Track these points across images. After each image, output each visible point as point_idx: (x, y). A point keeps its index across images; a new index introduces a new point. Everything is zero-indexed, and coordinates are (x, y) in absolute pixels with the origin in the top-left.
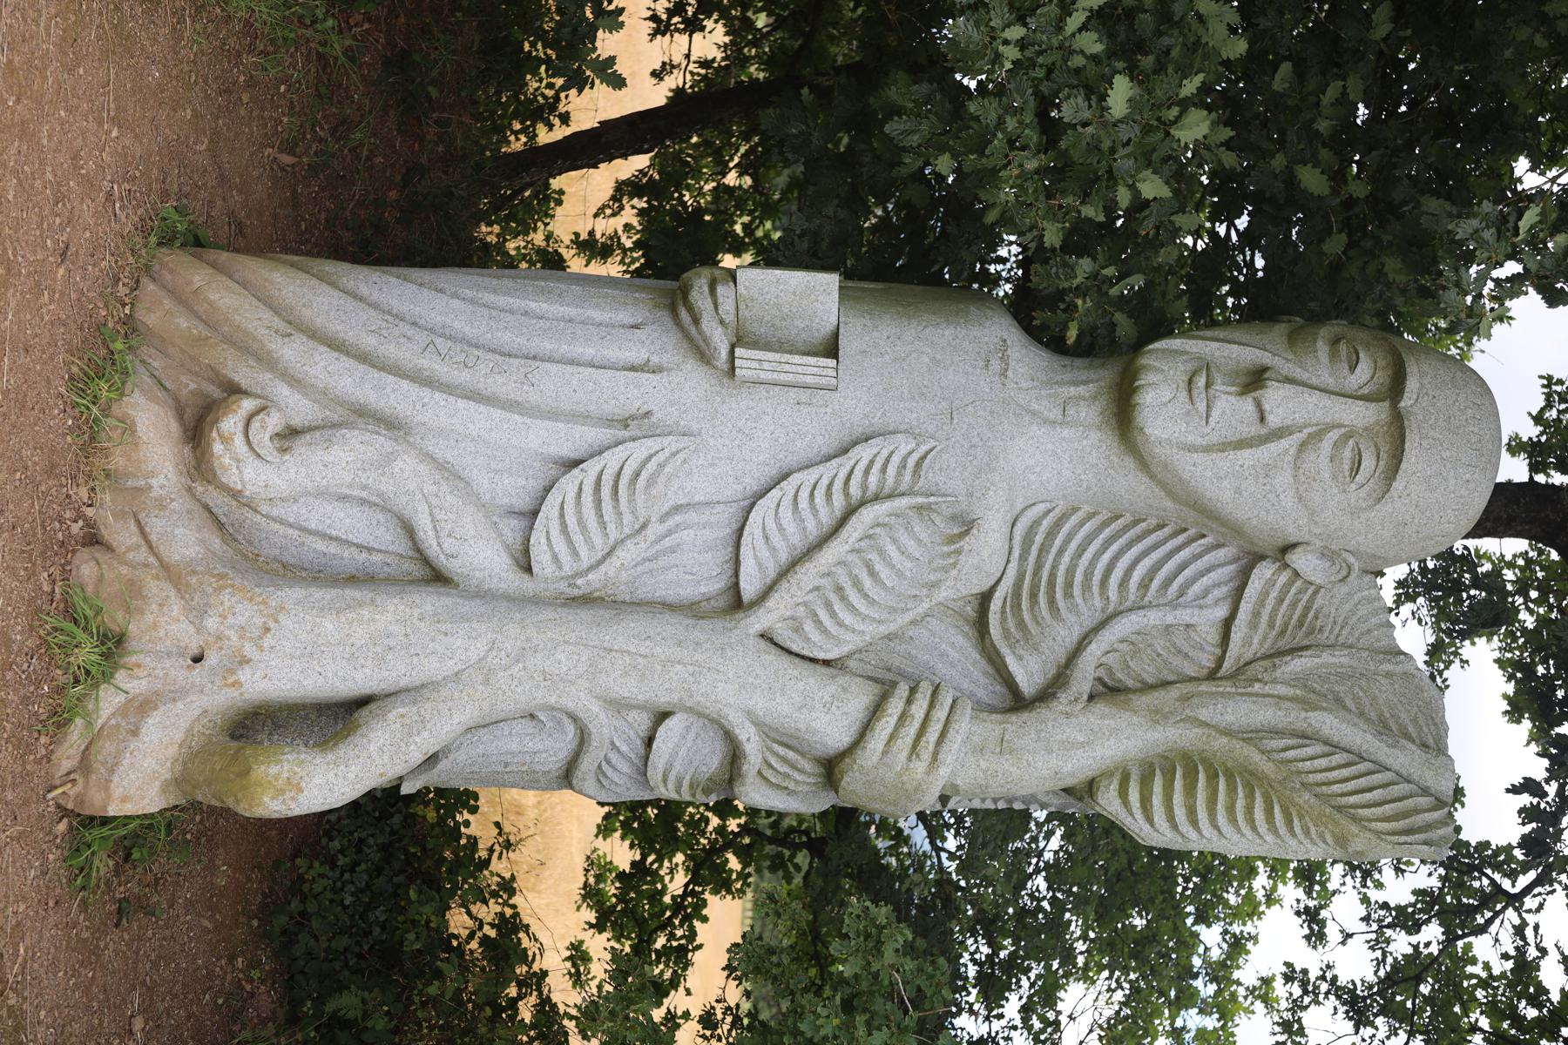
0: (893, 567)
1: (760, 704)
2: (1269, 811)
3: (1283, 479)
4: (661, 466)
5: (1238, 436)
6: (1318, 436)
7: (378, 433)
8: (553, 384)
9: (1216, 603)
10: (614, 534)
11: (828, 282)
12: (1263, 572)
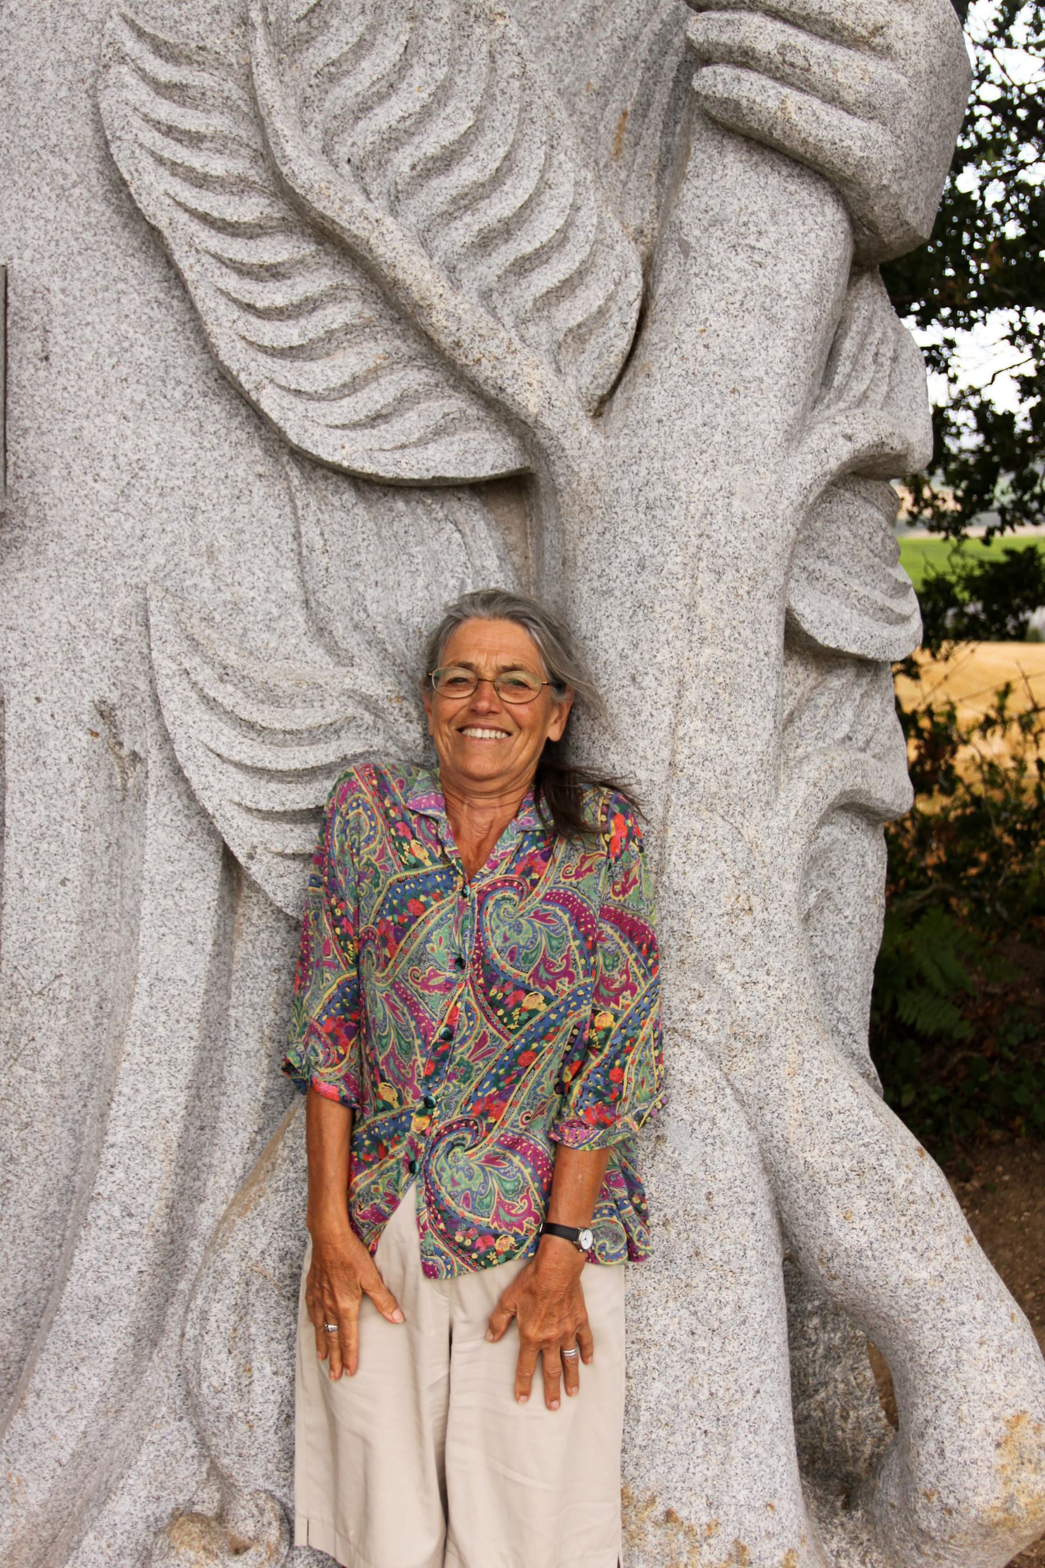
1: (769, 413)
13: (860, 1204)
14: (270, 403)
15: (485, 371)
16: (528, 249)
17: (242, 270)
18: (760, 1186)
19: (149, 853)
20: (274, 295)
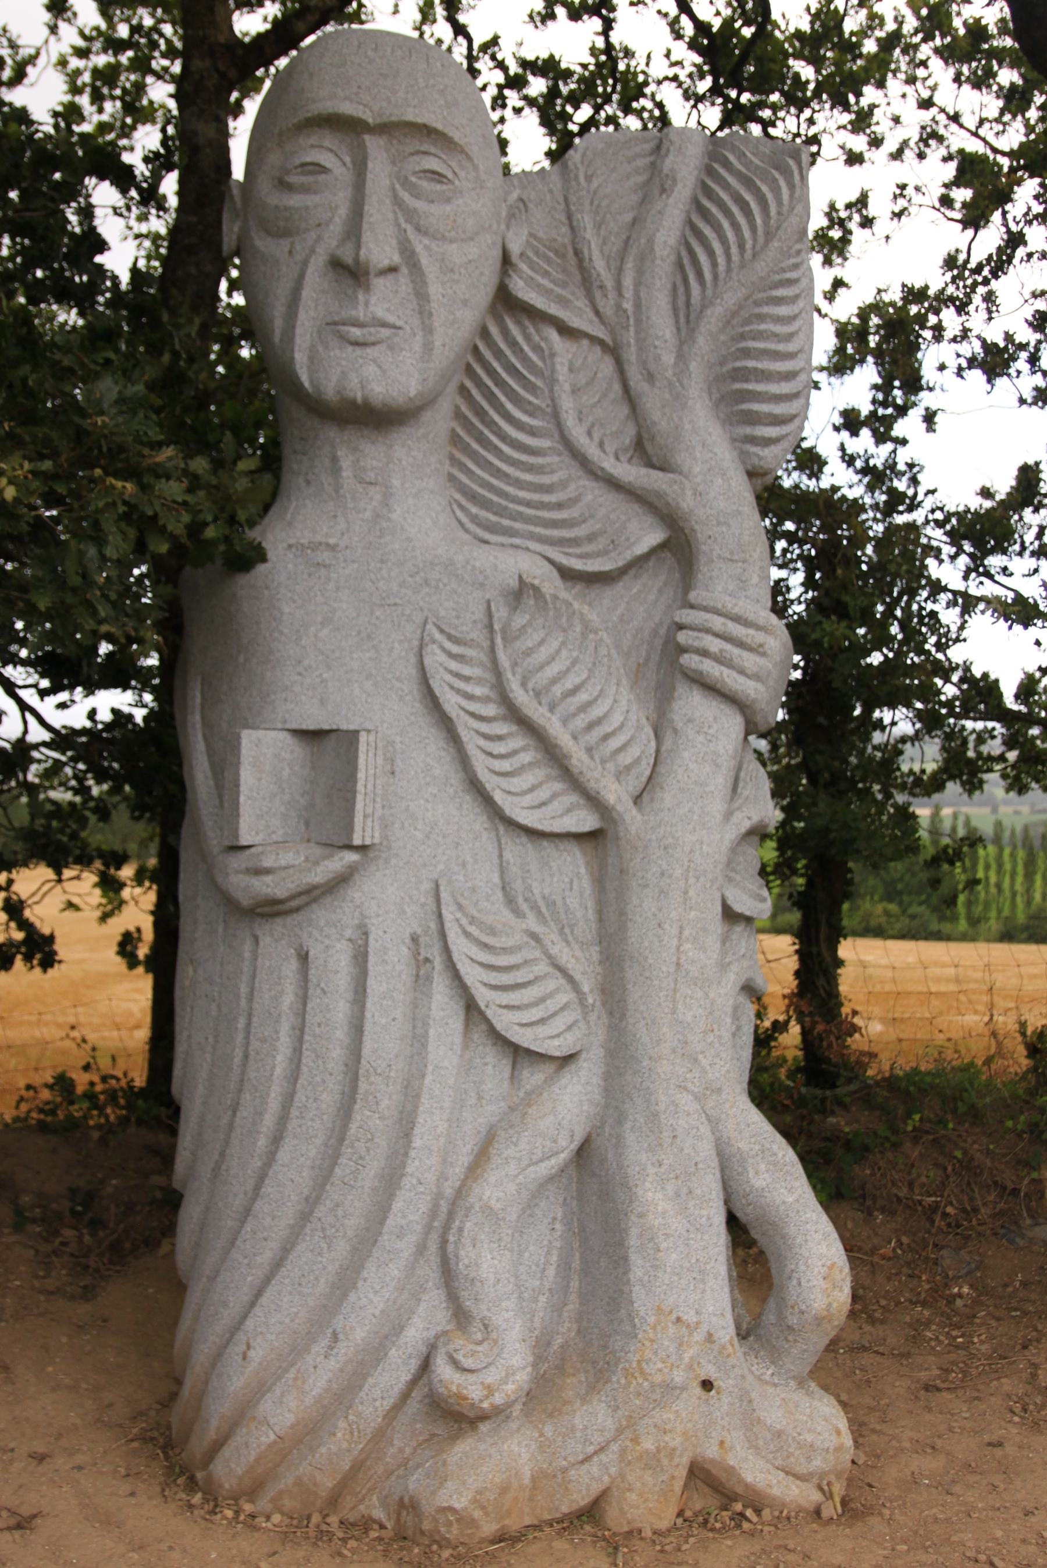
0: (568, 670)
1: (717, 807)
2: (779, 301)
3: (455, 253)
4: (473, 921)
5: (412, 297)
6: (410, 214)
7: (461, 1230)
8: (384, 1040)
9: (545, 339)
10: (542, 968)
11: (248, 738)
12: (519, 288)
13: (763, 1167)
14: (498, 797)
15: (592, 784)
16: (609, 730)
17: (486, 737)
18: (714, 1163)
19: (434, 1006)
20: (499, 748)
